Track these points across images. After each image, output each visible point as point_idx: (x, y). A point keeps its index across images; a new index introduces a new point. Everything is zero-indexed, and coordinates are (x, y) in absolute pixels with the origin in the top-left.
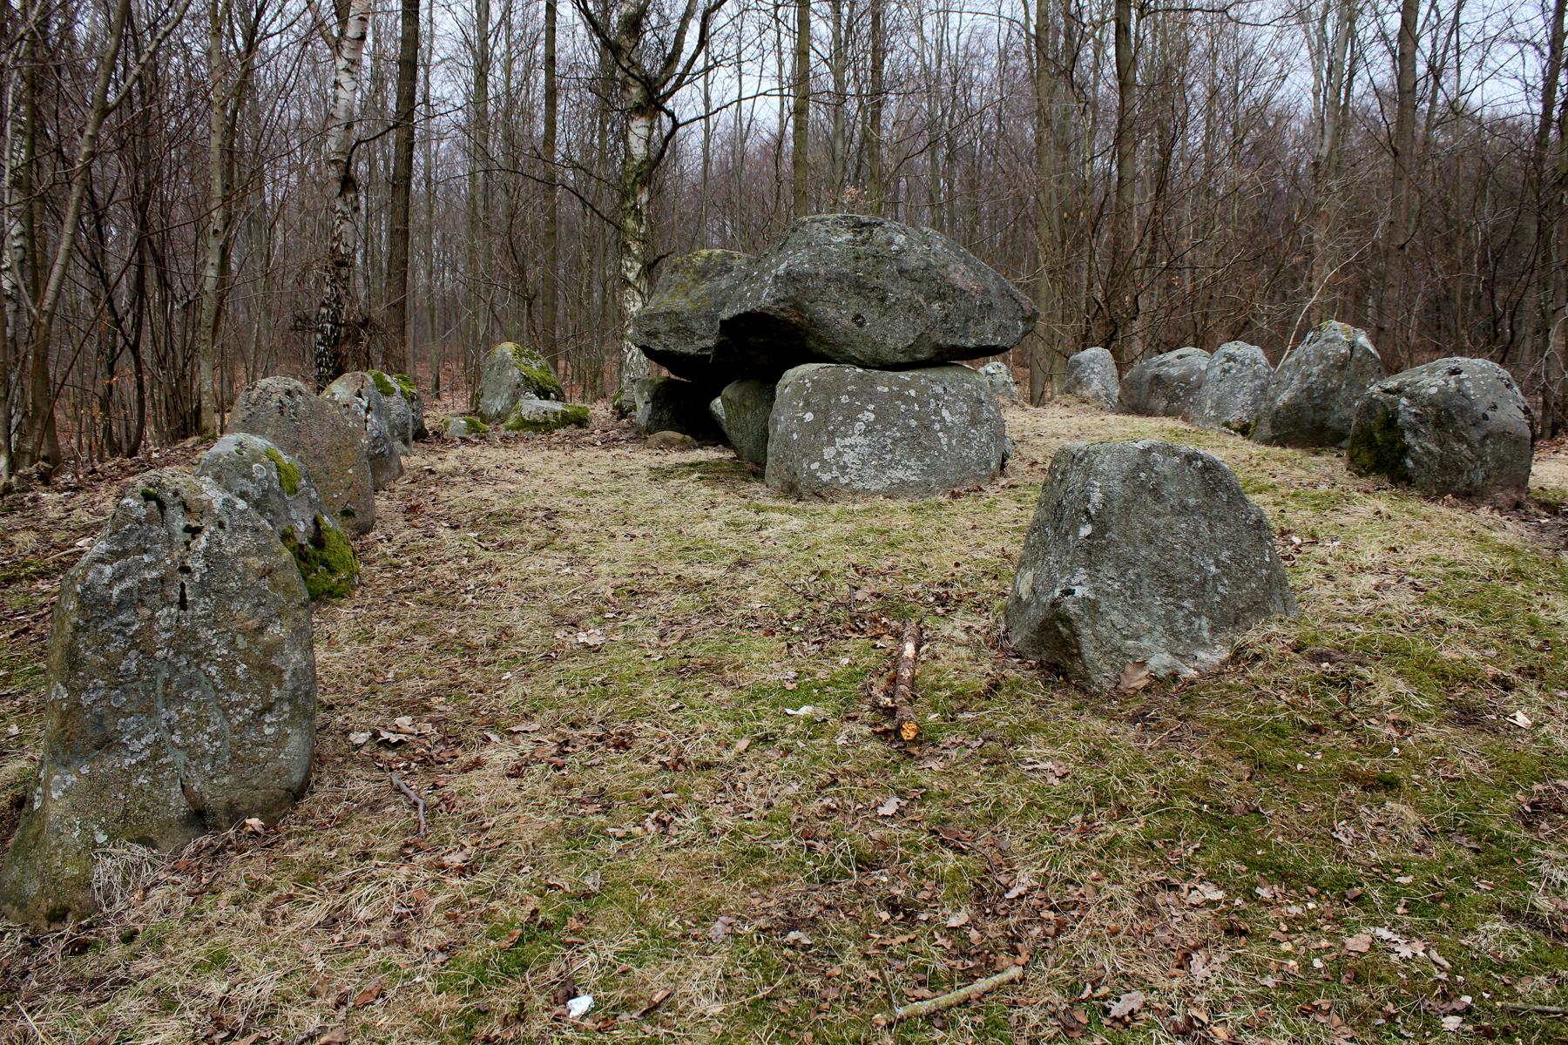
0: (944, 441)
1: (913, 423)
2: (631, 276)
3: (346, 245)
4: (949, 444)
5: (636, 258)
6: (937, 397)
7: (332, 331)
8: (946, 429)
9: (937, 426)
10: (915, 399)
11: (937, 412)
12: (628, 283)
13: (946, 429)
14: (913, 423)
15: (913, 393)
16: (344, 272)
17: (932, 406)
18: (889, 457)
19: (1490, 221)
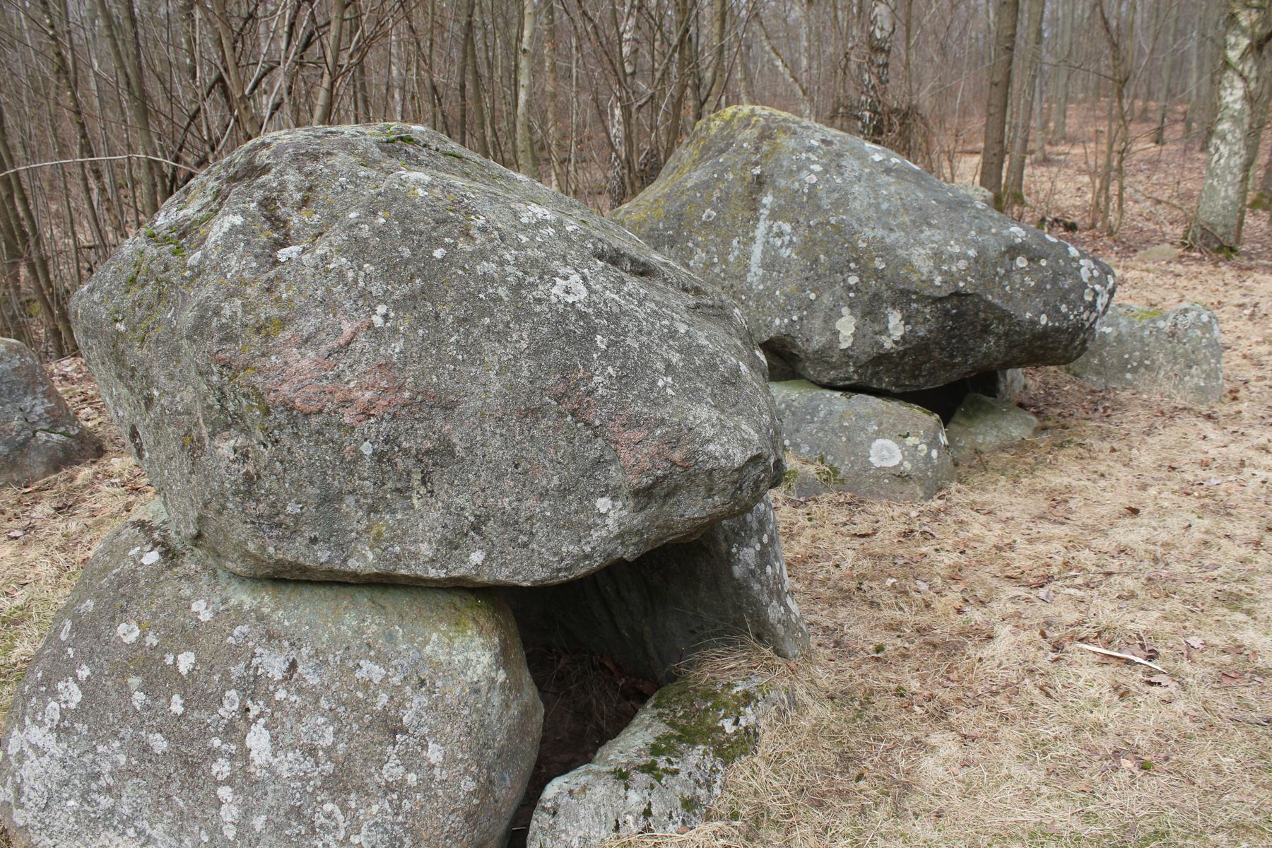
0: (229, 813)
1: (159, 743)
2: (1233, 55)
3: (882, 29)
4: (242, 825)
5: (1244, 31)
6: (254, 686)
7: (871, 119)
8: (244, 781)
9: (221, 768)
10: (183, 684)
11: (232, 731)
12: (1227, 65)
13: (244, 781)
14: (159, 743)
15: (186, 662)
16: (881, 59)
17: (230, 706)
18: (105, 802)
19: (341, 154)
